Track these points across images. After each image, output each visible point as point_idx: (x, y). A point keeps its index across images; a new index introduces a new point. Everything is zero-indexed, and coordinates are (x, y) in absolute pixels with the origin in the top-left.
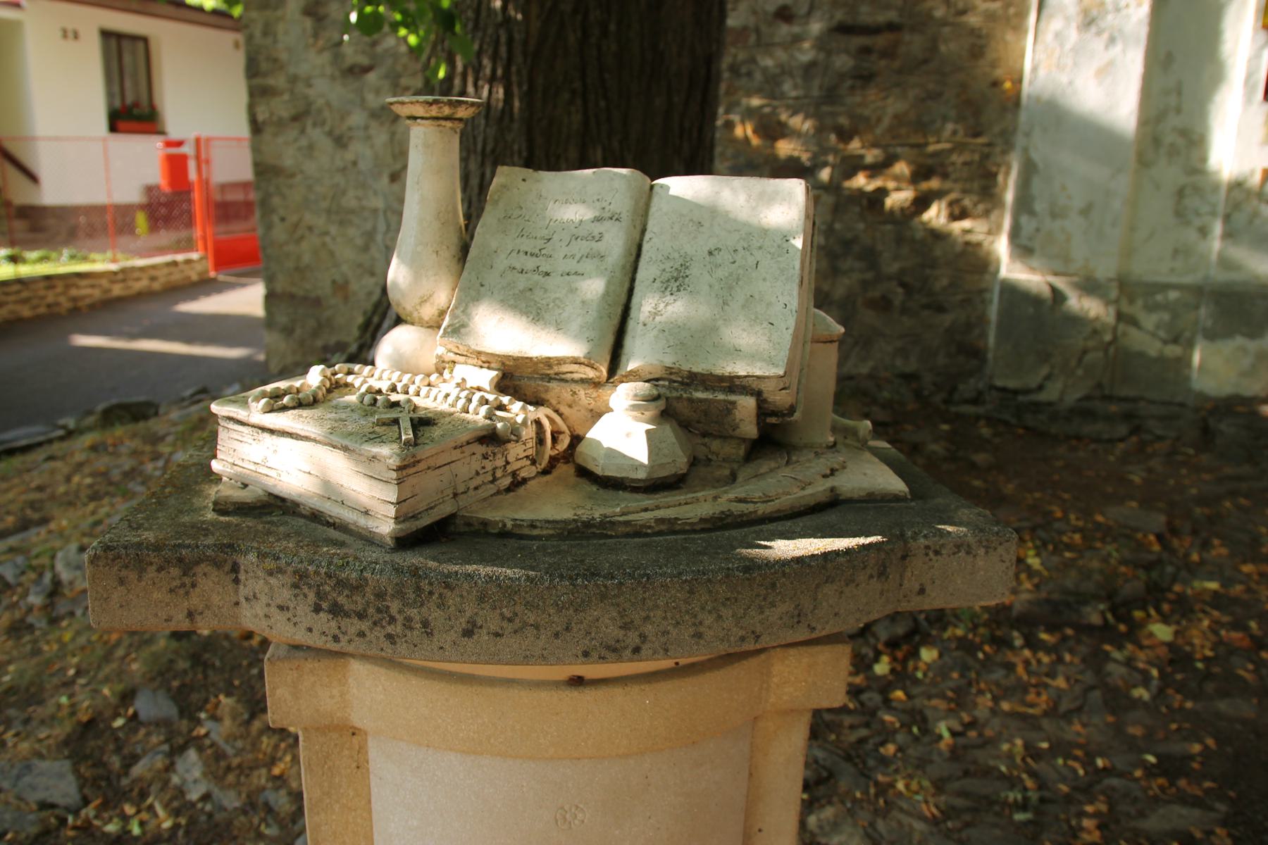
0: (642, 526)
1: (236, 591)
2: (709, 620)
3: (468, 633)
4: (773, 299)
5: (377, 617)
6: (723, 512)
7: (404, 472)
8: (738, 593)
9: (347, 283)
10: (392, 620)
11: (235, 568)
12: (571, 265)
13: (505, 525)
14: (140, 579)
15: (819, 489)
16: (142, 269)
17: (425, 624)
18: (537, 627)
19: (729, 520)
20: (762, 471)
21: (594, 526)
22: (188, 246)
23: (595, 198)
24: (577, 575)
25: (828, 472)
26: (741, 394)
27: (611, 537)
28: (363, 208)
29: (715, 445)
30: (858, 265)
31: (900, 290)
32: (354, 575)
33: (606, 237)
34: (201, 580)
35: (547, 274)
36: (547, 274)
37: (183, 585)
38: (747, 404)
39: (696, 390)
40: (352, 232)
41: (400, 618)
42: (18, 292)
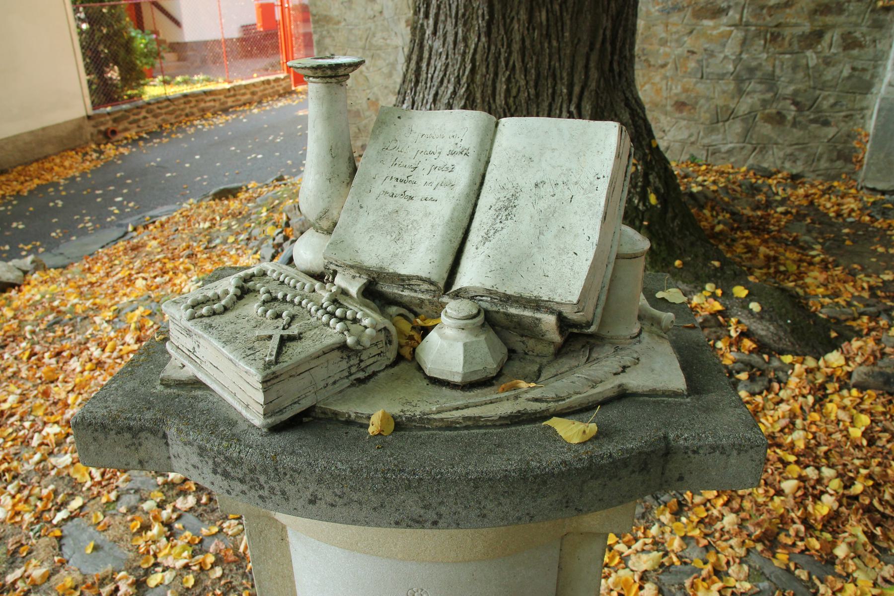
0: (452, 422)
1: (168, 450)
2: (490, 506)
3: (312, 502)
4: (580, 232)
5: (252, 483)
6: (519, 412)
7: (269, 384)
8: (514, 488)
9: (377, 100)
10: (262, 487)
11: (165, 436)
12: (428, 192)
13: (350, 416)
14: (106, 439)
15: (608, 387)
16: (246, 87)
17: (283, 493)
18: (360, 503)
19: (524, 417)
20: (563, 370)
21: (415, 421)
22: (274, 67)
23: (451, 134)
24: (389, 470)
25: (620, 369)
26: (546, 312)
27: (428, 429)
28: (388, 45)
29: (531, 343)
30: (760, 87)
31: (793, 108)
32: (235, 455)
33: (457, 168)
34: (145, 443)
35: (411, 198)
36: (411, 198)
37: (134, 444)
38: (549, 321)
39: (511, 306)
40: (380, 63)
41: (266, 487)
42: (167, 107)
